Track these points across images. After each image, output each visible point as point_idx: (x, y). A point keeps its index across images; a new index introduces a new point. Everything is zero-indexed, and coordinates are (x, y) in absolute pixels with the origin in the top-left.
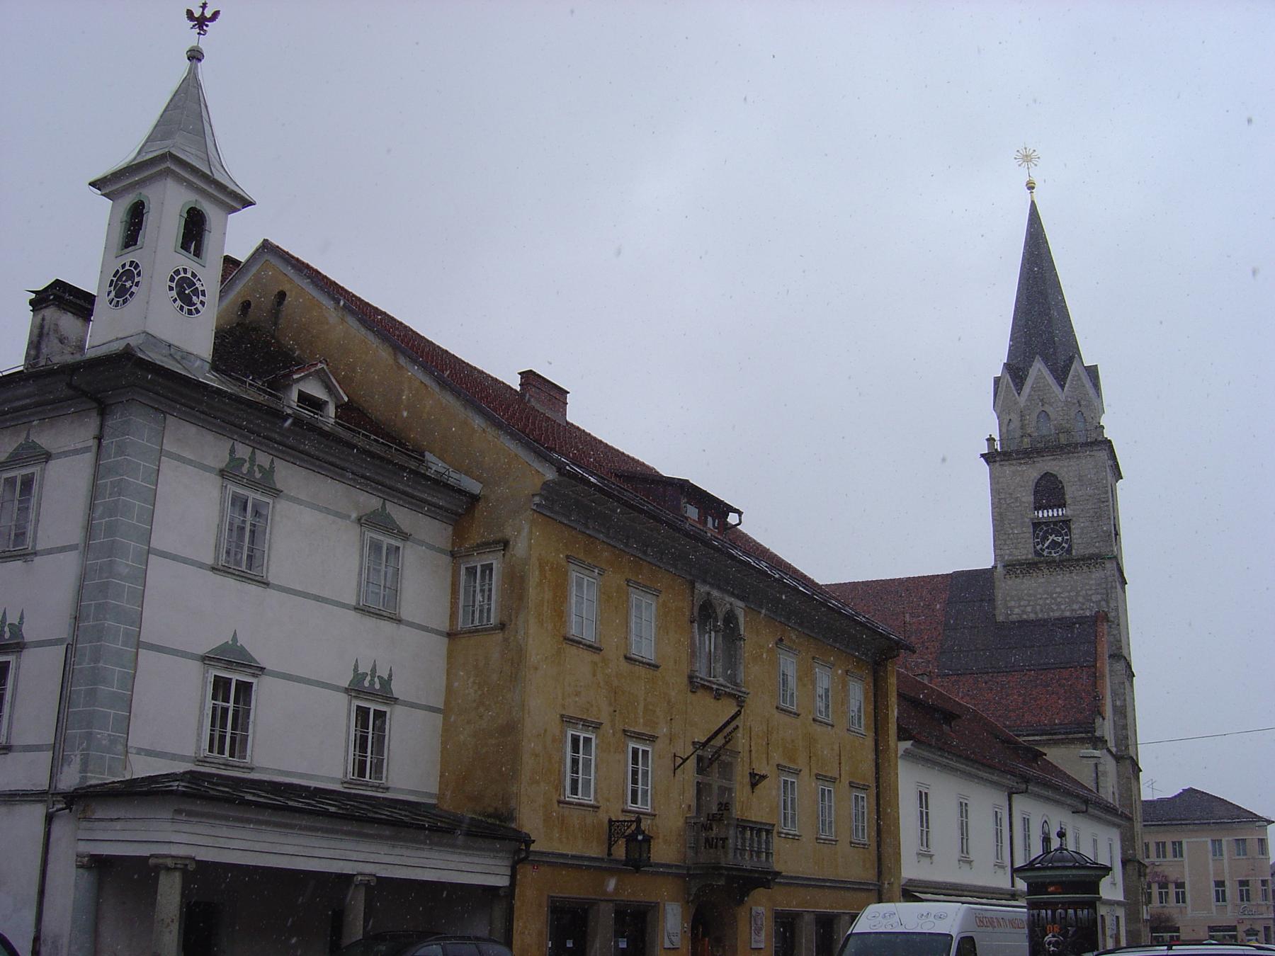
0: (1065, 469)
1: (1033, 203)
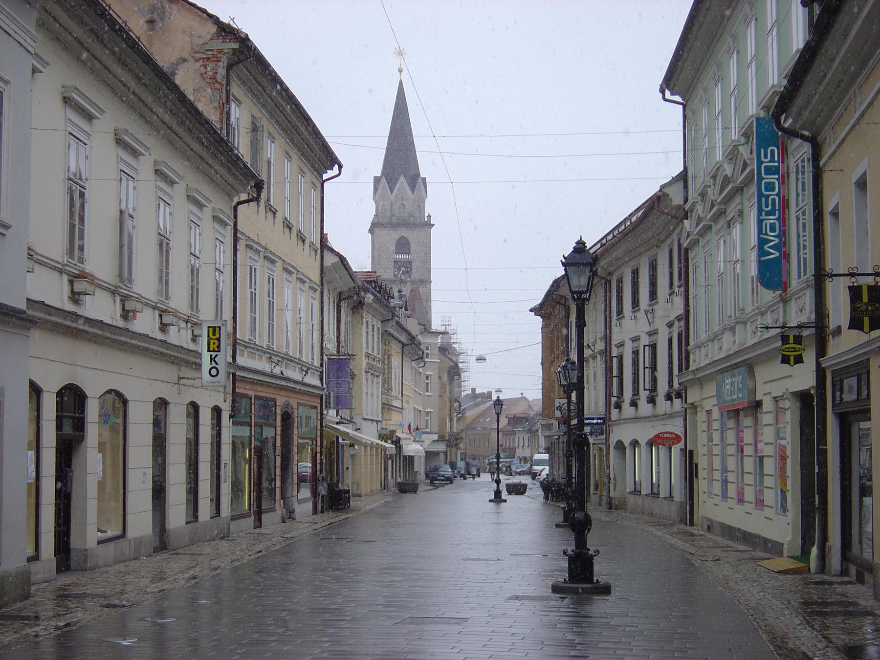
0: (412, 236)
1: (401, 83)
